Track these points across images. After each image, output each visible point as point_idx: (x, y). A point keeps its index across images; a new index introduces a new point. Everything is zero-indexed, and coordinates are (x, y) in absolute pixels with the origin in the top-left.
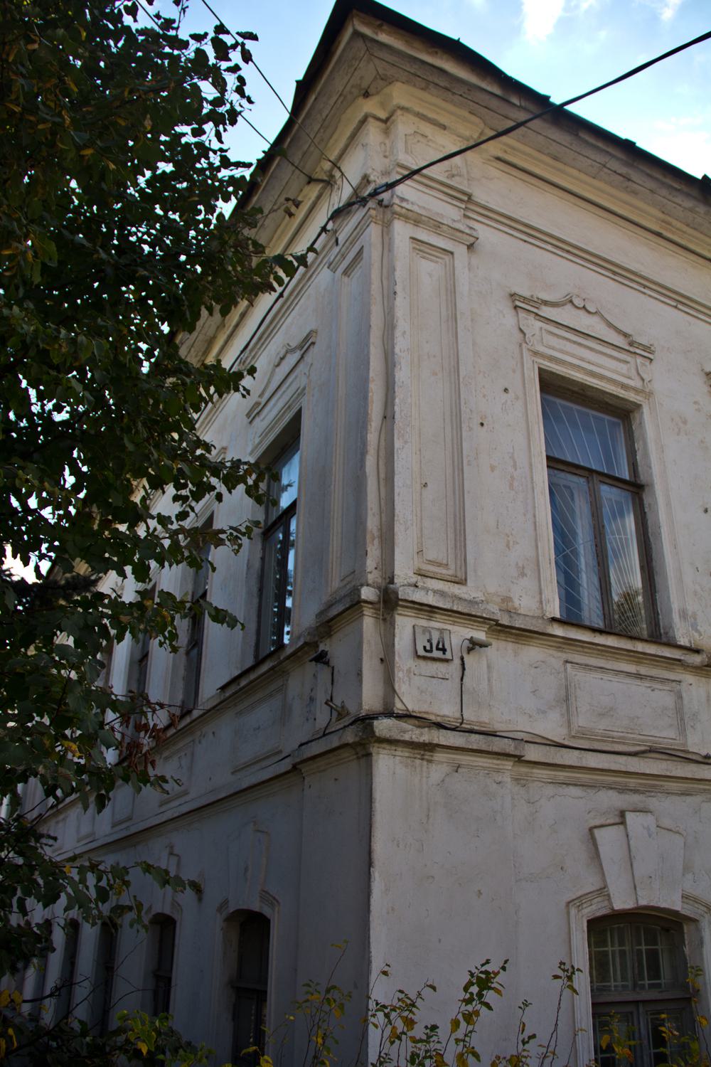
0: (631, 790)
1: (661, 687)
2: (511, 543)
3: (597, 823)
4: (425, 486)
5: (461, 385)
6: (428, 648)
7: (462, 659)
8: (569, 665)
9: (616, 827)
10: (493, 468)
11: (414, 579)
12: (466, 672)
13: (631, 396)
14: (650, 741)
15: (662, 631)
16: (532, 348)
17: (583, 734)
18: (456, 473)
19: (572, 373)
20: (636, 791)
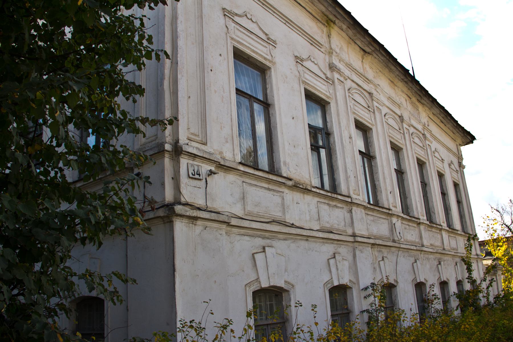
0: (266, 238)
1: (276, 194)
2: (222, 127)
3: (255, 251)
4: (189, 97)
5: (204, 51)
6: (193, 174)
7: (206, 179)
8: (244, 183)
9: (262, 253)
10: (215, 92)
11: (187, 141)
12: (208, 185)
13: (267, 63)
14: (273, 217)
15: (276, 170)
16: (231, 36)
17: (250, 214)
18: (202, 93)
19: (241, 47)
20: (268, 238)
